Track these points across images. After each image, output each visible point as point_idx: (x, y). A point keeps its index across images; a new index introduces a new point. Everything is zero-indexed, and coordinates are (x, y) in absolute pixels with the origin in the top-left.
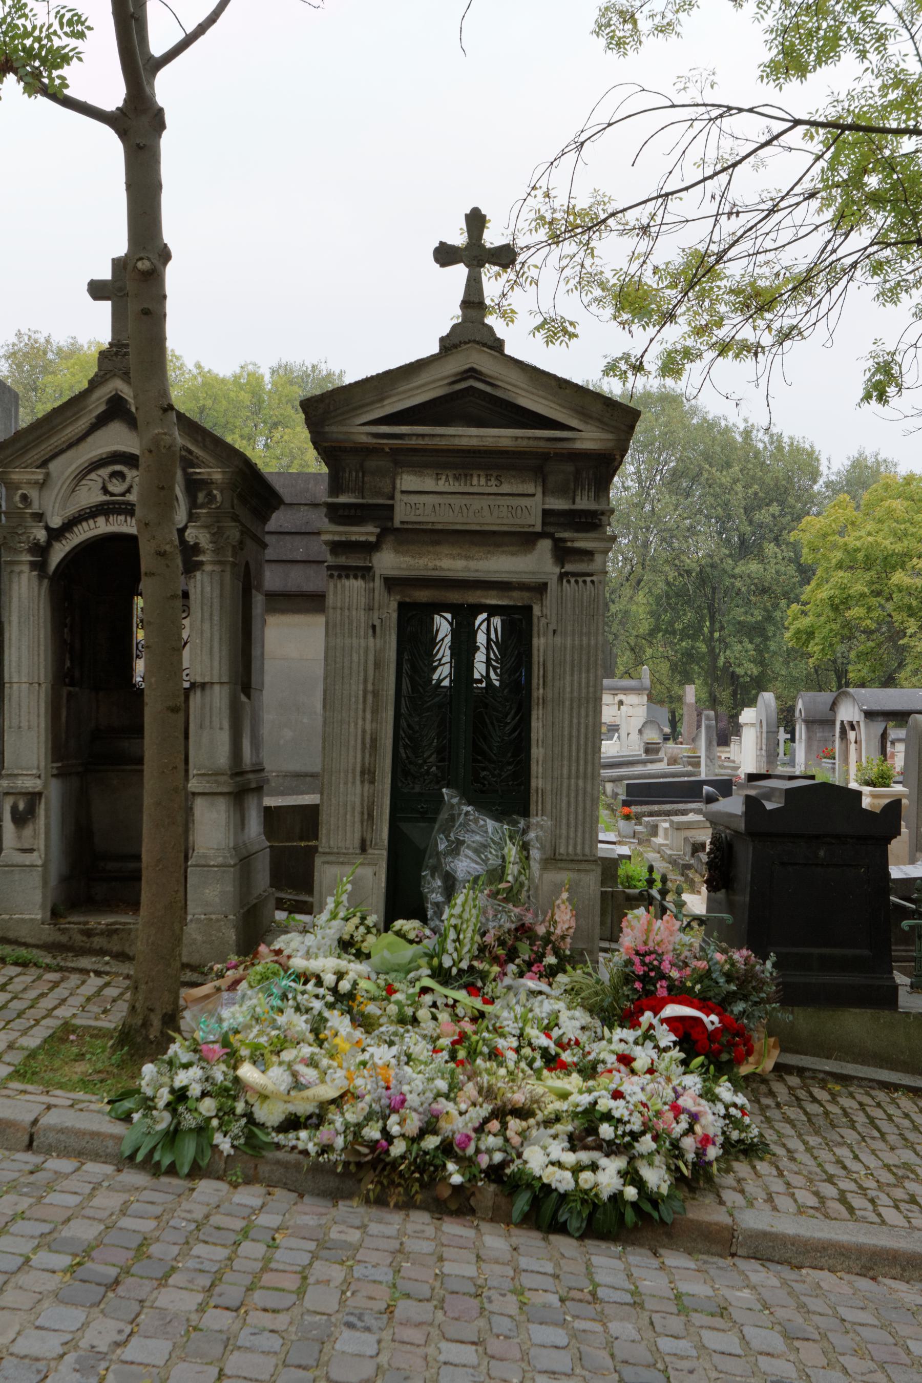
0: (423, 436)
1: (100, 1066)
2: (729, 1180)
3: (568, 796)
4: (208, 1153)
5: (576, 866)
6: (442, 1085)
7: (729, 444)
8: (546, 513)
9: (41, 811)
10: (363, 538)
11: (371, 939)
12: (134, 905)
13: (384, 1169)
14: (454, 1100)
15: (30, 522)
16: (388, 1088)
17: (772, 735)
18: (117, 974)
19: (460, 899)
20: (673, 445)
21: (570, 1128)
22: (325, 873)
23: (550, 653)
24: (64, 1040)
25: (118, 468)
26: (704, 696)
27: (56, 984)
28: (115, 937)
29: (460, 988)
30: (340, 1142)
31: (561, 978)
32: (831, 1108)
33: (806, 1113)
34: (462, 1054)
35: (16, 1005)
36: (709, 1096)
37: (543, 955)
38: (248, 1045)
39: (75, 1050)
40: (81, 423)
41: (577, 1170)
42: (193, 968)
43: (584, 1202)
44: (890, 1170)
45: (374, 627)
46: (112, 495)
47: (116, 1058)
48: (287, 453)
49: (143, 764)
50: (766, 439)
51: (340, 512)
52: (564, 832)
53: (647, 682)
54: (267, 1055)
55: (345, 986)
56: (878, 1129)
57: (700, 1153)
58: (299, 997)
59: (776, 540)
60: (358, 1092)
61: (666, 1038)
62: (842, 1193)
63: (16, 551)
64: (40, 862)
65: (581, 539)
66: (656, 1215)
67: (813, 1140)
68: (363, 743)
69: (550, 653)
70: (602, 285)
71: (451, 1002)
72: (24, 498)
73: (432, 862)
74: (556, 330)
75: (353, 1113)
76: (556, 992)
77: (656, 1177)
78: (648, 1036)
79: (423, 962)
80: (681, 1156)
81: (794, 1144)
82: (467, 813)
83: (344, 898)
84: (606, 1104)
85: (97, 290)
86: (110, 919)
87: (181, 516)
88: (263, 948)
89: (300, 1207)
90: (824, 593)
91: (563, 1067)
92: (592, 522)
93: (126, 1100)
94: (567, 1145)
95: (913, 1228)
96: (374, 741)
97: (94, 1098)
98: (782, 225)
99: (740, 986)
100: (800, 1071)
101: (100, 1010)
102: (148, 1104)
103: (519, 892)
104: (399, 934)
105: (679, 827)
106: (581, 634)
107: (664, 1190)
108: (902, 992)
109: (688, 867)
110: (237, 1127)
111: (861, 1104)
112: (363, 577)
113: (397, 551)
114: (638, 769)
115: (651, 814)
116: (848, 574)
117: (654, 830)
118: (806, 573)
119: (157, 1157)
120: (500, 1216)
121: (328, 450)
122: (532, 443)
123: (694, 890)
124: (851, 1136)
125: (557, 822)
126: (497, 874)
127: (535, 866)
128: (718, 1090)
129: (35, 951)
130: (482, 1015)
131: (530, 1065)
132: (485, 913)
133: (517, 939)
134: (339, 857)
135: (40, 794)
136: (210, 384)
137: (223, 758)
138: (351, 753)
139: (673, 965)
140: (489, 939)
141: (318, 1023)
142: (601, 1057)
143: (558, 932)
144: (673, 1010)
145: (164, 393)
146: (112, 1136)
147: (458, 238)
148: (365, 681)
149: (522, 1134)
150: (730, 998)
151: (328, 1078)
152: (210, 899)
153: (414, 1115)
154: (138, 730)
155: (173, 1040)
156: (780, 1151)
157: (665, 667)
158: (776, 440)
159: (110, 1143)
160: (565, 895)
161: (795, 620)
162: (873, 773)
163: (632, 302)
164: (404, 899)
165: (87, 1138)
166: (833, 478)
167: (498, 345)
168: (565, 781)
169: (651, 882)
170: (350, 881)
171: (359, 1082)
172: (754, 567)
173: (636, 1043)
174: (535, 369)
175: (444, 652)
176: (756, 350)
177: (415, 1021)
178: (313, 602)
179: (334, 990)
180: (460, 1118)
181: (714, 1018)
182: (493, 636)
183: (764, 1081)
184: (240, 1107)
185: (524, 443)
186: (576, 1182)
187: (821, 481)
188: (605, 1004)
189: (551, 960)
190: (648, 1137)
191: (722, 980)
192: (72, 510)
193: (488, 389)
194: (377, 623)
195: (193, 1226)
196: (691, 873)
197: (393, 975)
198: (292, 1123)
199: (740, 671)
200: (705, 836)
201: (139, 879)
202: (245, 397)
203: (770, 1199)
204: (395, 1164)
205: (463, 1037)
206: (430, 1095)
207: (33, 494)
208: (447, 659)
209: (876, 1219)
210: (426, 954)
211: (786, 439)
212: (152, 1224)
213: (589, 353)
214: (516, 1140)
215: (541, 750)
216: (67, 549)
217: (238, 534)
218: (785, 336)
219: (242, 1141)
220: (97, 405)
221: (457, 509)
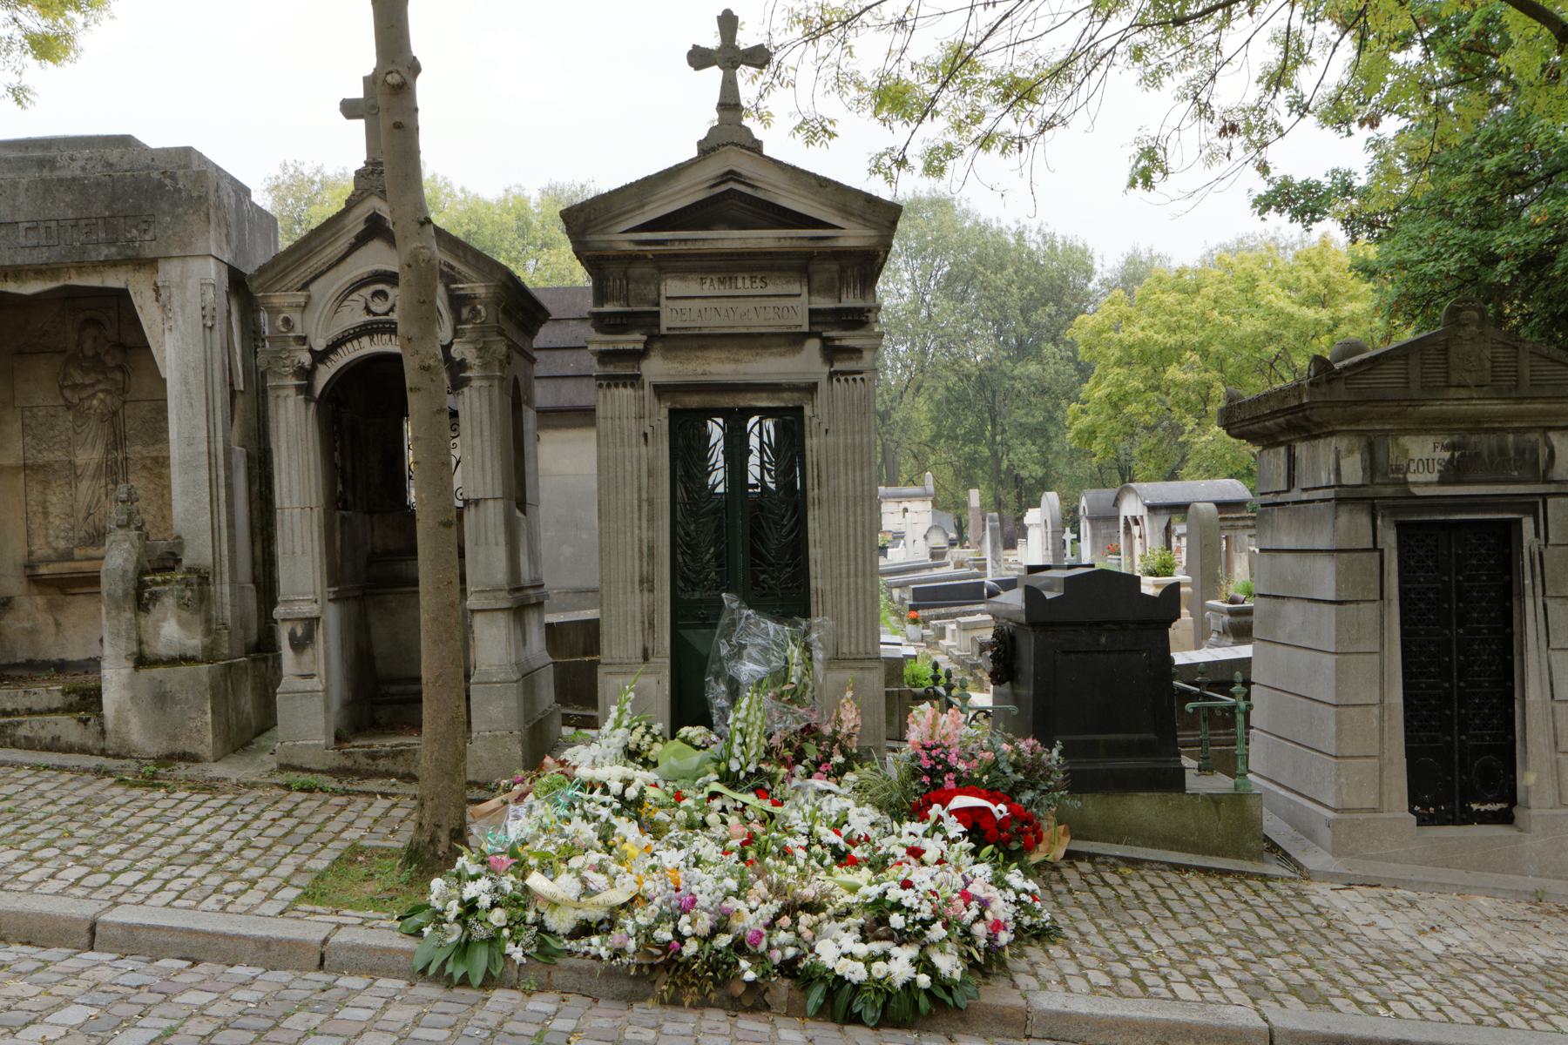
0: (686, 241)
1: (389, 884)
2: (1022, 964)
3: (848, 594)
4: (501, 963)
5: (859, 665)
6: (732, 884)
7: (1002, 248)
8: (812, 312)
9: (319, 636)
10: (630, 347)
11: (658, 747)
12: (416, 726)
13: (677, 970)
14: (745, 899)
15: (293, 345)
16: (678, 890)
17: (1057, 534)
18: (405, 795)
19: (744, 703)
20: (946, 249)
21: (861, 920)
22: (607, 683)
23: (823, 451)
24: (352, 862)
25: (379, 287)
26: (990, 500)
27: (343, 808)
28: (400, 758)
29: (748, 791)
30: (632, 945)
31: (850, 777)
32: (1123, 891)
33: (1098, 897)
34: (751, 854)
35: (304, 830)
36: (1002, 884)
37: (831, 755)
38: (535, 855)
39: (364, 871)
40: (340, 243)
41: (869, 960)
42: (481, 786)
43: (877, 991)
44: (1182, 948)
45: (645, 435)
46: (375, 314)
47: (405, 876)
48: (553, 269)
49: (417, 584)
50: (1039, 239)
51: (606, 321)
52: (845, 631)
53: (931, 488)
54: (556, 864)
55: (631, 793)
56: (1170, 910)
57: (992, 938)
58: (586, 806)
59: (1054, 340)
60: (648, 895)
61: (955, 828)
62: (1135, 971)
63: (281, 376)
64: (321, 687)
65: (849, 337)
66: (950, 1001)
67: (1105, 923)
68: (641, 552)
69: (823, 451)
70: (859, 85)
71: (740, 805)
72: (287, 321)
73: (715, 667)
74: (817, 131)
75: (643, 917)
76: (846, 791)
77: (948, 963)
78: (937, 827)
79: (711, 767)
80: (972, 943)
81: (1087, 927)
82: (748, 617)
83: (628, 706)
84: (895, 893)
85: (350, 109)
86: (395, 741)
87: (445, 333)
88: (548, 760)
89: (595, 1011)
90: (1100, 393)
91: (855, 863)
92: (859, 319)
93: (416, 917)
94: (858, 936)
95: (1205, 1001)
96: (651, 549)
97: (384, 916)
98: (1039, 13)
99: (1027, 776)
100: (1091, 857)
101: (387, 831)
102: (438, 918)
103: (804, 693)
104: (685, 740)
105: (965, 628)
106: (853, 432)
107: (957, 975)
108: (1188, 774)
109: (976, 666)
110: (528, 936)
111: (1152, 886)
112: (632, 385)
113: (665, 358)
114: (925, 574)
115: (938, 618)
116: (1124, 371)
117: (941, 633)
118: (1084, 371)
119: (449, 969)
120: (795, 1011)
121: (593, 261)
122: (795, 243)
123: (981, 688)
124: (1142, 917)
125: (838, 619)
126: (781, 676)
127: (817, 666)
128: (1008, 877)
129: (320, 776)
130: (772, 816)
131: (820, 862)
132: (770, 715)
133: (804, 740)
134: (623, 668)
135: (318, 619)
136: (476, 209)
137: (500, 574)
138: (629, 563)
139: (959, 757)
140: (776, 741)
141: (608, 833)
142: (891, 851)
143: (844, 730)
144: (960, 802)
145: (420, 204)
146: (403, 951)
147: (711, 40)
148: (640, 490)
149: (813, 928)
150: (1018, 788)
151: (617, 883)
152: (496, 716)
153: (706, 915)
154: (413, 552)
155: (460, 854)
156: (1073, 935)
157: (948, 473)
158: (1049, 240)
159: (402, 958)
160: (849, 694)
161: (1076, 418)
162: (1155, 563)
163: (893, 99)
164: (689, 706)
165: (378, 954)
166: (1108, 275)
167: (755, 147)
168: (845, 581)
169: (936, 679)
170: (633, 690)
171: (648, 885)
172: (1033, 368)
173: (925, 835)
174: (794, 169)
175: (718, 457)
176: (1021, 142)
177: (705, 825)
178: (582, 416)
179: (621, 798)
180: (751, 916)
181: (1002, 807)
182: (765, 439)
183: (1056, 869)
184: (531, 916)
185: (788, 243)
186: (869, 972)
187: (1095, 279)
188: (893, 800)
189: (838, 759)
190: (939, 924)
191: (1009, 770)
192: (335, 332)
193: (749, 191)
194: (649, 430)
195: (487, 1033)
196: (979, 673)
197: (682, 782)
198: (584, 929)
199: (1024, 473)
200: (988, 635)
201: (420, 701)
202: (510, 220)
203: (1063, 981)
204: (687, 965)
205: (751, 839)
206: (720, 894)
207: (295, 317)
208: (720, 464)
209: (1169, 995)
210: (713, 760)
211: (1059, 239)
212: (446, 1033)
213: (851, 155)
214: (808, 934)
215: (819, 551)
216: (333, 371)
217: (504, 349)
218: (1047, 125)
219: (534, 949)
220: (355, 224)
221: (723, 312)
